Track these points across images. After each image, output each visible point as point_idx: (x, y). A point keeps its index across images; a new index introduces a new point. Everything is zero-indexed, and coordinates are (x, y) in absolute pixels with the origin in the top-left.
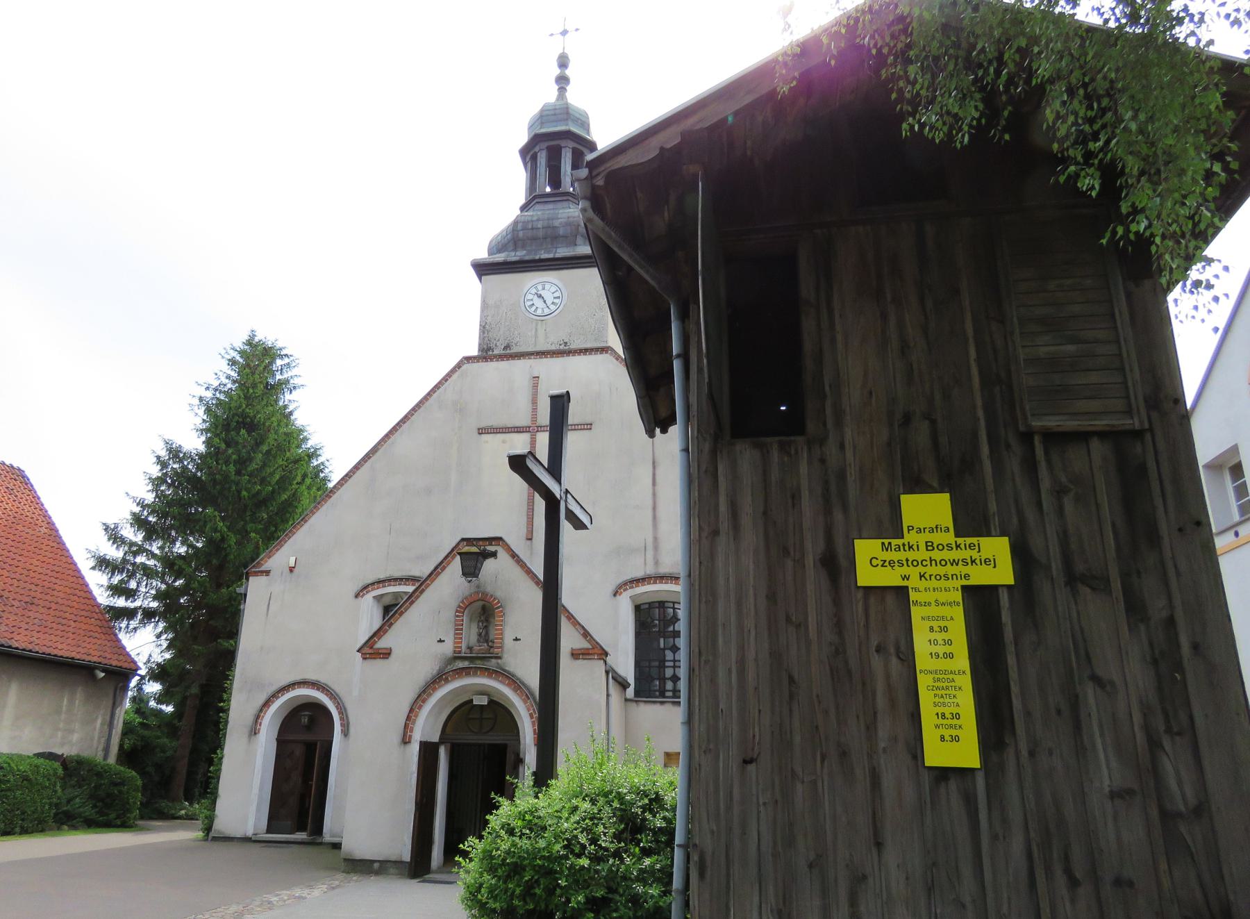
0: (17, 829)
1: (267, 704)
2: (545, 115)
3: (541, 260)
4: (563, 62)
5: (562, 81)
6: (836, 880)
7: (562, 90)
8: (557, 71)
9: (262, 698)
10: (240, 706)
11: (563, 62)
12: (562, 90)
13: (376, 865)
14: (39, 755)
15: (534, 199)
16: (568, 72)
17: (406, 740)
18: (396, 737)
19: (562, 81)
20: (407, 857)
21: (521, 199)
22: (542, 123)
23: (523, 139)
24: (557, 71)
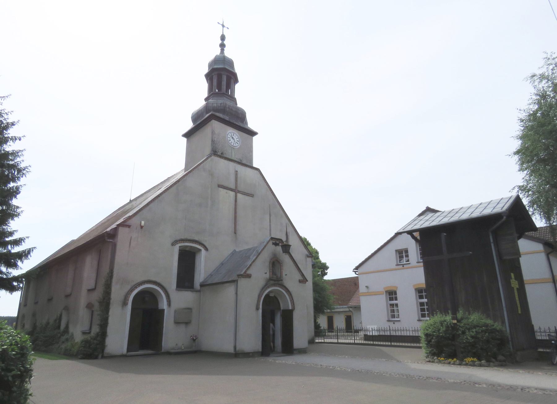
1: (131, 290)
2: (216, 60)
4: (223, 38)
5: (222, 46)
7: (222, 51)
8: (220, 42)
9: (128, 287)
10: (117, 292)
11: (223, 38)
12: (222, 51)
13: (251, 354)
14: (305, 243)
15: (212, 94)
16: (225, 42)
19: (222, 46)
20: (260, 350)
21: (206, 95)
22: (215, 63)
23: (206, 70)
24: (220, 42)
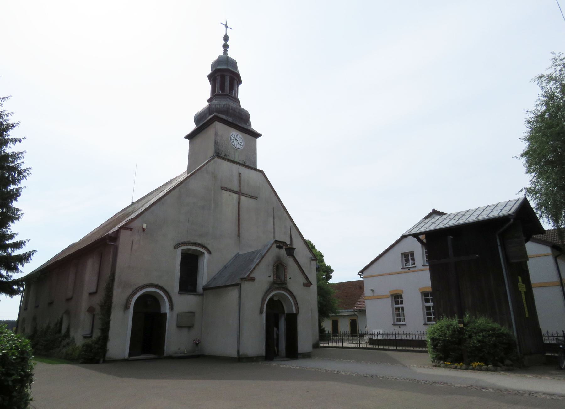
0: (102, 360)
3: (237, 125)
4: (226, 38)
5: (226, 46)
6: (278, 339)
8: (224, 42)
10: (119, 296)
11: (226, 38)
12: (226, 51)
17: (261, 313)
18: (258, 312)
19: (226, 46)
20: (264, 354)
21: (209, 96)
23: (209, 71)
24: (224, 42)
